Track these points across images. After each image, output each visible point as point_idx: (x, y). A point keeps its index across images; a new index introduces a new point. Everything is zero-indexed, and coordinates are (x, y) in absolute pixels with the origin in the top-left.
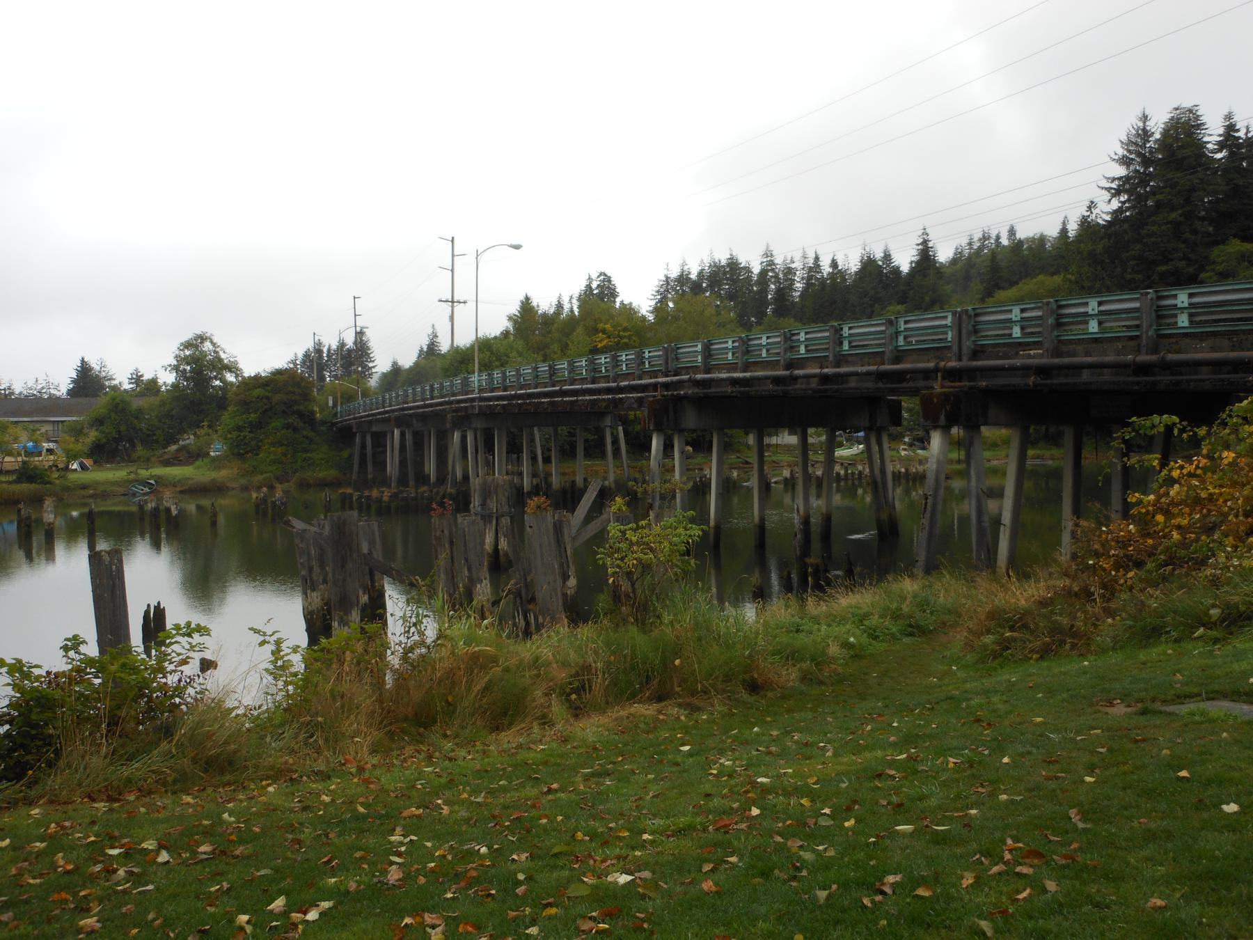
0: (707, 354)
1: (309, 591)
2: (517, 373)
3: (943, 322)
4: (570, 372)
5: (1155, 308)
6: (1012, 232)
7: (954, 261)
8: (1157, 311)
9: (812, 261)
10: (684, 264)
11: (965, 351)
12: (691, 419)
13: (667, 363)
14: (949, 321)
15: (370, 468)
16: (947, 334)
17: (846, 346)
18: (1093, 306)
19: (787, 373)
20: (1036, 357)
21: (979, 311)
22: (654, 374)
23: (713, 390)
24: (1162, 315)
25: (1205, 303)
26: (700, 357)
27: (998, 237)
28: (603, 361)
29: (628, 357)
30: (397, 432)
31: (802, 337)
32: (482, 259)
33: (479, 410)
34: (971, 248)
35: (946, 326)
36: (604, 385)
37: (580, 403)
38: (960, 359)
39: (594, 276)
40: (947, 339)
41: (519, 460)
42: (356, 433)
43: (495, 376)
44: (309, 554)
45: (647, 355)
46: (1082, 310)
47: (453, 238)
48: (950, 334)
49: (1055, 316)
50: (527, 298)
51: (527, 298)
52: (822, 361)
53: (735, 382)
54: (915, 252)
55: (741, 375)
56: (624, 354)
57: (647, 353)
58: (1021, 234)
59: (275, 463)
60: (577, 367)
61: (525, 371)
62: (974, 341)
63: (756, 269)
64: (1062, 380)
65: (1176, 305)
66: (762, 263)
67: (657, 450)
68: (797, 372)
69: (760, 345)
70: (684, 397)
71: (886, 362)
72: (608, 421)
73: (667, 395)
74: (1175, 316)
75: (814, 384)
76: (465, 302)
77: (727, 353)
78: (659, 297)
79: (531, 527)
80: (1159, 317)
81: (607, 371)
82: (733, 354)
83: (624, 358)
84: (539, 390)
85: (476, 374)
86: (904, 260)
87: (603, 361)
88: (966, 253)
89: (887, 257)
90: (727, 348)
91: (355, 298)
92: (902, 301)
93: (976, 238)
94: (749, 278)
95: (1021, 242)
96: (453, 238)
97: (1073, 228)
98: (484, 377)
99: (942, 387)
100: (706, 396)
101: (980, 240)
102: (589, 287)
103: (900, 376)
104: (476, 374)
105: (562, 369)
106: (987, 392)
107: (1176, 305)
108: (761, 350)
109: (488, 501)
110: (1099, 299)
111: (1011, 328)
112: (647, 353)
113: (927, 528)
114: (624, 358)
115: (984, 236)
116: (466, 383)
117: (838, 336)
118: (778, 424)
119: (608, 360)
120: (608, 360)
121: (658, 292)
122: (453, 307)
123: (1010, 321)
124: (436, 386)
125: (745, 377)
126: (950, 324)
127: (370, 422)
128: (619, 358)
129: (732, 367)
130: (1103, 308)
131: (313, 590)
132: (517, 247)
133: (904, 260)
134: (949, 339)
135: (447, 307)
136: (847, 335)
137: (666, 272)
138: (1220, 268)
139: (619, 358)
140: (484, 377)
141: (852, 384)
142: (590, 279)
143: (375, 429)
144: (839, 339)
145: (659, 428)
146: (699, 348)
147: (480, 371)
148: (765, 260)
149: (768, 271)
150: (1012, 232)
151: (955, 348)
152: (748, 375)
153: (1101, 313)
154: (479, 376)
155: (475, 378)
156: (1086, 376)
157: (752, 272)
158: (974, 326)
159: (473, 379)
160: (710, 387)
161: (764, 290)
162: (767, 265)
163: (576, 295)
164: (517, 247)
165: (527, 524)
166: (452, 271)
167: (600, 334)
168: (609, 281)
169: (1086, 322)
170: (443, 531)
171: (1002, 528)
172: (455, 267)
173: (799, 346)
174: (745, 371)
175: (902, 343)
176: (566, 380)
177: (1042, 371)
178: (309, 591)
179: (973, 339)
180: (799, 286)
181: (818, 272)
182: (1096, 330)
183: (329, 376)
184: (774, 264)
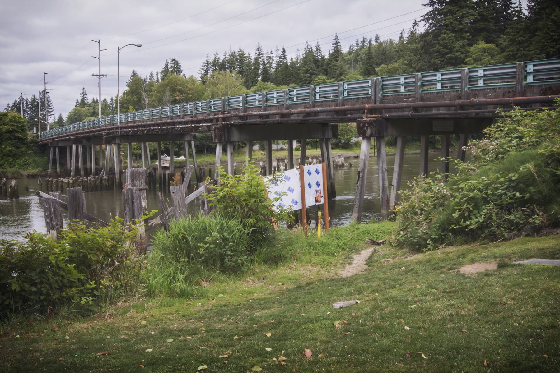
0: (245, 102)
1: (51, 230)
2: (142, 114)
3: (367, 85)
4: (171, 113)
5: (468, 77)
6: (377, 38)
7: (350, 53)
8: (469, 78)
9: (281, 53)
10: (217, 54)
11: (378, 99)
12: (236, 137)
13: (224, 107)
14: (370, 84)
15: (58, 166)
16: (368, 90)
17: (318, 97)
18: (439, 76)
19: (421, 103)
20: (410, 101)
21: (384, 79)
22: (216, 113)
23: (248, 121)
24: (472, 80)
25: (543, 69)
26: (241, 104)
27: (370, 40)
28: (189, 106)
29: (202, 104)
30: (74, 147)
31: (295, 92)
32: (121, 52)
33: (120, 133)
34: (357, 46)
35: (368, 87)
36: (518, 98)
37: (176, 129)
38: (375, 103)
39: (169, 61)
40: (368, 93)
41: (226, 155)
42: (50, 147)
43: (129, 115)
44: (50, 210)
45: (212, 103)
46: (433, 78)
47: (99, 40)
48: (370, 90)
49: (421, 81)
50: (134, 73)
51: (134, 73)
52: (306, 106)
53: (261, 116)
54: (332, 48)
55: (264, 113)
56: (200, 103)
57: (213, 102)
58: (382, 39)
59: (28, 164)
60: (175, 110)
61: (146, 113)
62: (382, 94)
63: (253, 57)
64: (424, 113)
65: (478, 75)
66: (256, 53)
67: (219, 153)
68: (293, 111)
69: (273, 97)
70: (232, 125)
71: (339, 105)
72: (187, 138)
73: (224, 124)
74: (477, 81)
75: (277, 118)
76: (106, 76)
77: (256, 102)
78: (203, 72)
79: (173, 193)
80: (470, 81)
81: (191, 112)
82: (259, 102)
83: (200, 105)
84: (516, 98)
85: (119, 114)
86: (326, 51)
87: (189, 106)
88: (355, 49)
89: (318, 50)
90: (255, 99)
91: (45, 73)
92: (326, 73)
93: (360, 42)
94: (250, 62)
95: (381, 44)
96: (99, 40)
97: (406, 36)
98: (123, 116)
99: (367, 117)
100: (245, 124)
101: (362, 42)
102: (166, 67)
103: (344, 112)
104: (119, 114)
105: (166, 111)
106: (387, 120)
107: (478, 75)
108: (274, 100)
109: (135, 181)
110: (442, 73)
111: (400, 87)
112: (213, 102)
113: (360, 188)
114: (200, 105)
115: (364, 40)
116: (113, 119)
117: (314, 92)
118: (278, 137)
119: (191, 106)
120: (191, 106)
121: (203, 69)
122: (100, 78)
123: (399, 84)
124: (96, 121)
125: (486, 101)
126: (370, 86)
127: (58, 141)
128: (197, 105)
129: (259, 108)
130: (444, 77)
131: (53, 229)
132: (139, 46)
133: (326, 51)
134: (370, 93)
135: (96, 78)
136: (318, 91)
137: (207, 59)
138: (474, 56)
139: (197, 105)
140: (123, 116)
141: (321, 117)
142: (167, 62)
143: (60, 145)
144: (314, 93)
145: (220, 142)
146: (241, 99)
147: (121, 113)
148: (257, 52)
149: (259, 58)
150: (377, 38)
151: (373, 98)
152: (267, 112)
153: (443, 80)
154: (120, 115)
155: (118, 117)
156: (434, 112)
157: (251, 59)
158: (382, 86)
159: (117, 117)
160: (247, 119)
161: (257, 69)
162: (258, 55)
163: (161, 71)
164: (139, 46)
165: (172, 192)
166: (99, 58)
167: (177, 93)
168: (177, 64)
169: (436, 84)
170: (128, 196)
171: (392, 187)
172: (101, 57)
173: (293, 98)
174: (265, 111)
175: (346, 96)
176: (168, 117)
177: (415, 109)
178: (51, 230)
179: (381, 93)
180: (274, 65)
181: (284, 59)
182: (440, 88)
183: (27, 117)
184: (262, 54)
